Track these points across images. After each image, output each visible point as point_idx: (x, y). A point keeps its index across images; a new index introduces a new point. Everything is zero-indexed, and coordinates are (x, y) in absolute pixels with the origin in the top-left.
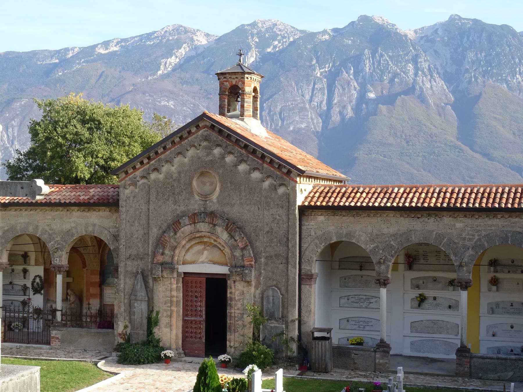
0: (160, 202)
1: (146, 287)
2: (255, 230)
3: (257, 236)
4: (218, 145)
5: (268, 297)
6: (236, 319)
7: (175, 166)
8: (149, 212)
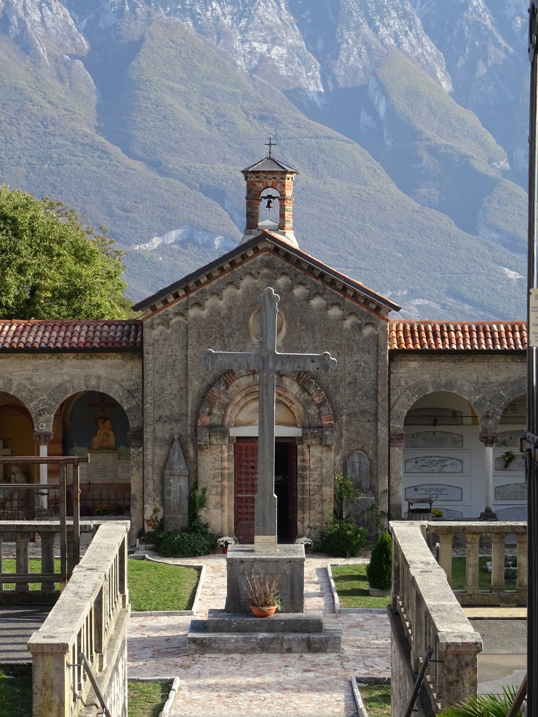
0: (202, 347)
1: (186, 457)
2: (334, 381)
3: (336, 388)
4: (284, 274)
5: (353, 463)
6: (312, 492)
7: (224, 299)
8: (187, 359)
